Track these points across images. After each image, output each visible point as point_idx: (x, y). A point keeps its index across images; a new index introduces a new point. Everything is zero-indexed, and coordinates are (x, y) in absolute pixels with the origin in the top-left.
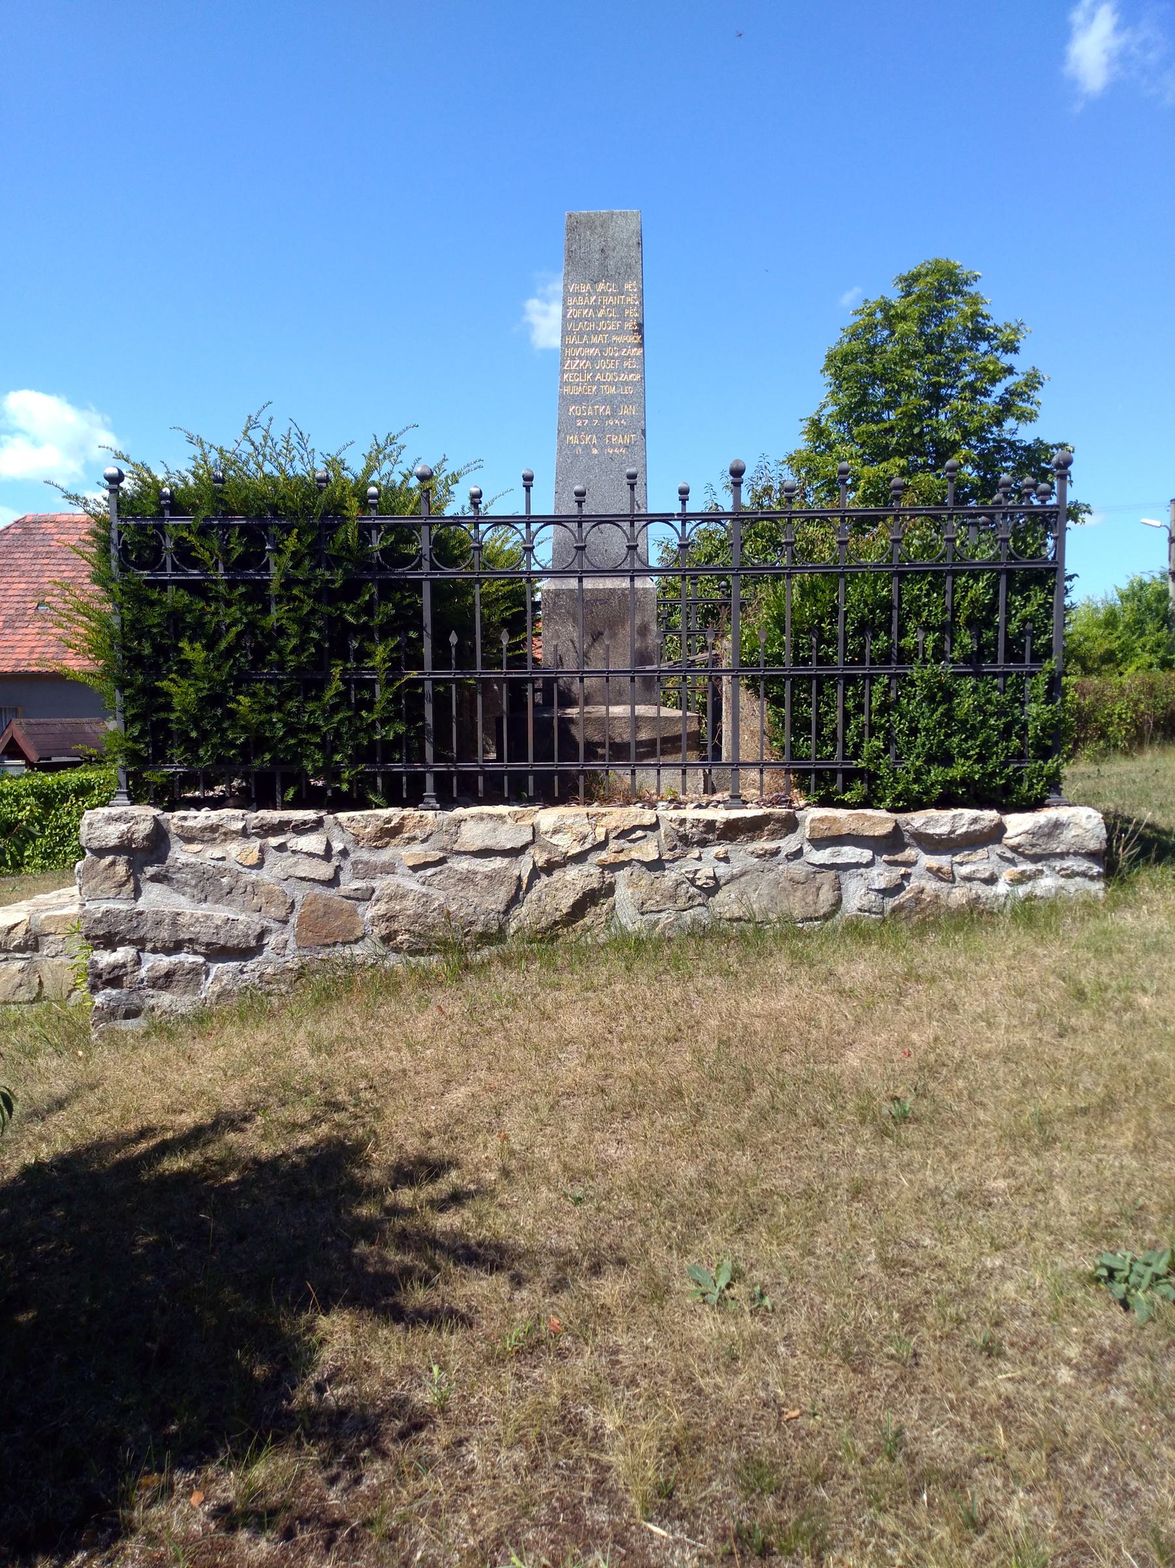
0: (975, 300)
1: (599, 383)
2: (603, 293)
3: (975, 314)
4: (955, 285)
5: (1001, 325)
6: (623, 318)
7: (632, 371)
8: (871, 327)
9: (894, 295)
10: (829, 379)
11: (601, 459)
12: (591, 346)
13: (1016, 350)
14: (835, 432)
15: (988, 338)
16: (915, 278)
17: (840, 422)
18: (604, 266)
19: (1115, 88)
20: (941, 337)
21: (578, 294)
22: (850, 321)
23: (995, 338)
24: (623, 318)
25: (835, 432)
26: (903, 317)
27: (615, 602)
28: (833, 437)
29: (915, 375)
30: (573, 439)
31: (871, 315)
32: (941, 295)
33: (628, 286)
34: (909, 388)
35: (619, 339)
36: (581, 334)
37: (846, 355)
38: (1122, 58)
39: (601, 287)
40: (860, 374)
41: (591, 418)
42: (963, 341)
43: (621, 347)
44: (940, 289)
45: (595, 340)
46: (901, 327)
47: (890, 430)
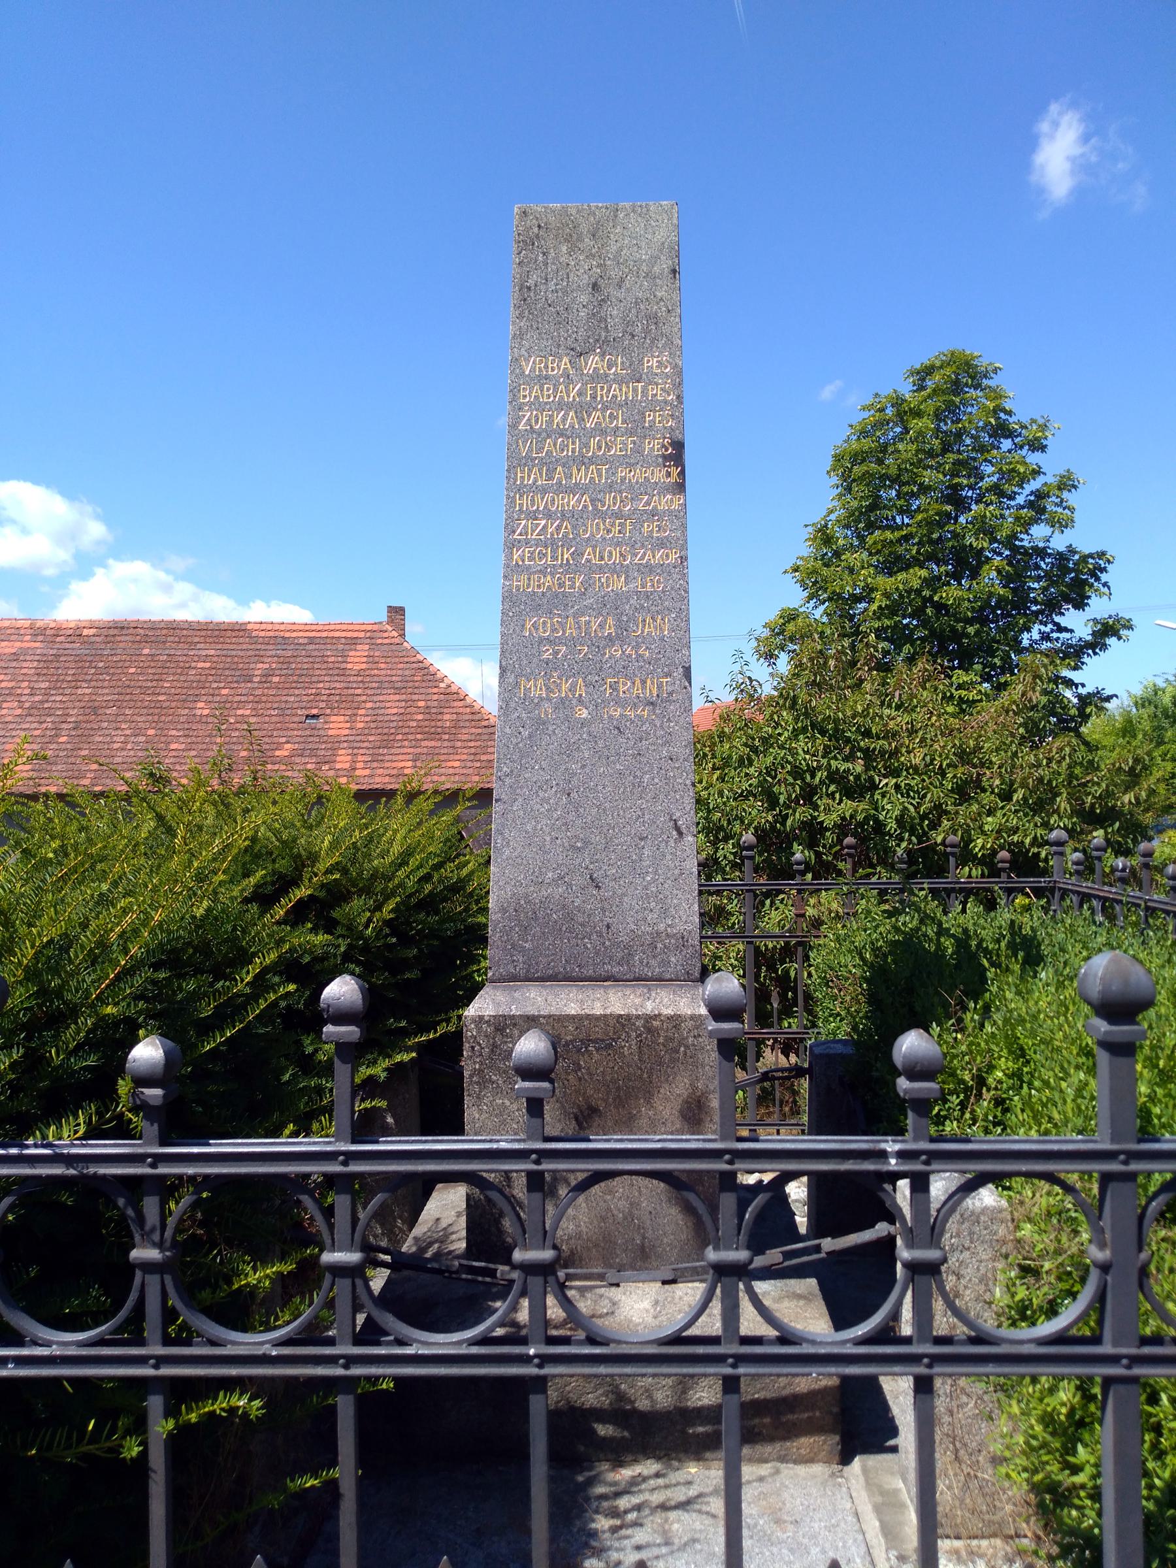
0: (997, 394)
1: (591, 569)
2: (596, 377)
3: (998, 409)
4: (973, 378)
5: (1025, 420)
6: (638, 429)
7: (662, 544)
8: (881, 424)
9: (906, 389)
10: (835, 480)
11: (596, 728)
12: (572, 490)
13: (1043, 448)
14: (842, 537)
15: (1010, 434)
16: (929, 370)
17: (847, 527)
18: (598, 318)
19: (1079, 193)
20: (959, 435)
21: (543, 379)
22: (858, 417)
23: (1020, 435)
24: (638, 429)
25: (842, 537)
26: (918, 414)
27: (629, 1047)
28: (841, 542)
29: (928, 477)
30: (536, 689)
31: (882, 410)
32: (956, 387)
33: (651, 362)
34: (924, 489)
35: (636, 475)
36: (549, 466)
37: (856, 454)
38: (1080, 166)
39: (593, 362)
40: (871, 475)
41: (571, 643)
42: (985, 438)
43: (636, 491)
44: (956, 383)
45: (580, 476)
46: (916, 424)
47: (907, 538)
